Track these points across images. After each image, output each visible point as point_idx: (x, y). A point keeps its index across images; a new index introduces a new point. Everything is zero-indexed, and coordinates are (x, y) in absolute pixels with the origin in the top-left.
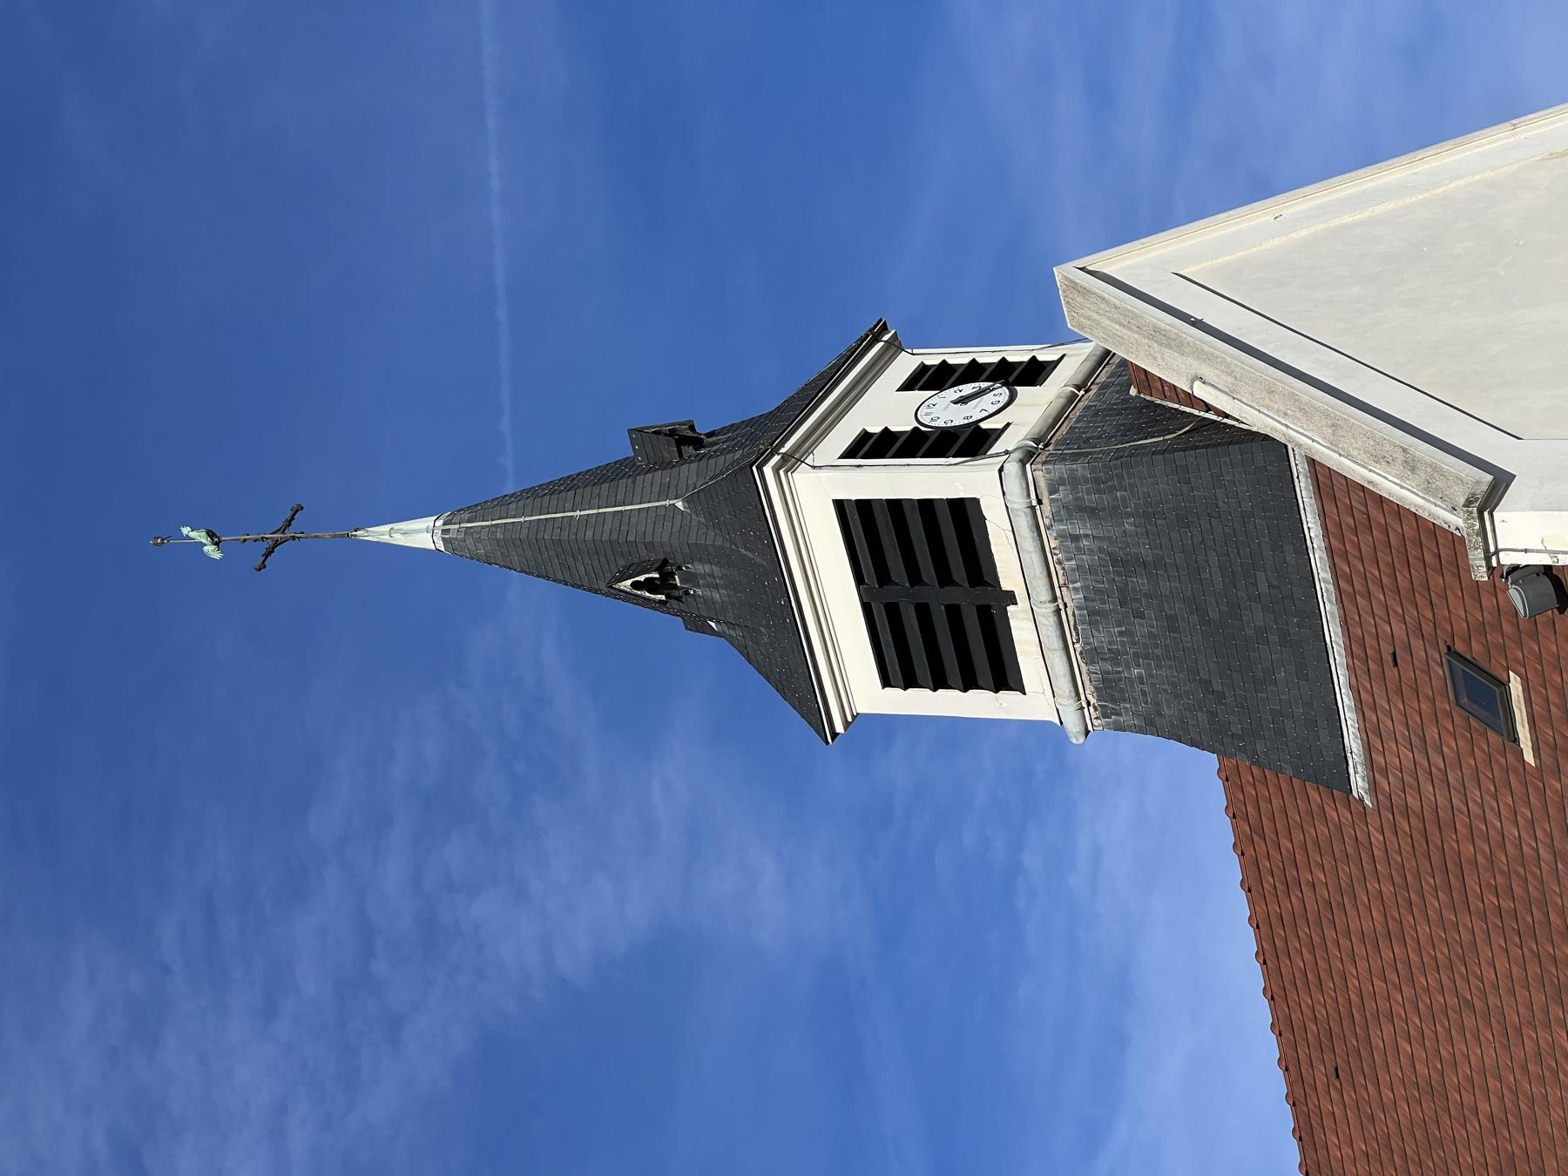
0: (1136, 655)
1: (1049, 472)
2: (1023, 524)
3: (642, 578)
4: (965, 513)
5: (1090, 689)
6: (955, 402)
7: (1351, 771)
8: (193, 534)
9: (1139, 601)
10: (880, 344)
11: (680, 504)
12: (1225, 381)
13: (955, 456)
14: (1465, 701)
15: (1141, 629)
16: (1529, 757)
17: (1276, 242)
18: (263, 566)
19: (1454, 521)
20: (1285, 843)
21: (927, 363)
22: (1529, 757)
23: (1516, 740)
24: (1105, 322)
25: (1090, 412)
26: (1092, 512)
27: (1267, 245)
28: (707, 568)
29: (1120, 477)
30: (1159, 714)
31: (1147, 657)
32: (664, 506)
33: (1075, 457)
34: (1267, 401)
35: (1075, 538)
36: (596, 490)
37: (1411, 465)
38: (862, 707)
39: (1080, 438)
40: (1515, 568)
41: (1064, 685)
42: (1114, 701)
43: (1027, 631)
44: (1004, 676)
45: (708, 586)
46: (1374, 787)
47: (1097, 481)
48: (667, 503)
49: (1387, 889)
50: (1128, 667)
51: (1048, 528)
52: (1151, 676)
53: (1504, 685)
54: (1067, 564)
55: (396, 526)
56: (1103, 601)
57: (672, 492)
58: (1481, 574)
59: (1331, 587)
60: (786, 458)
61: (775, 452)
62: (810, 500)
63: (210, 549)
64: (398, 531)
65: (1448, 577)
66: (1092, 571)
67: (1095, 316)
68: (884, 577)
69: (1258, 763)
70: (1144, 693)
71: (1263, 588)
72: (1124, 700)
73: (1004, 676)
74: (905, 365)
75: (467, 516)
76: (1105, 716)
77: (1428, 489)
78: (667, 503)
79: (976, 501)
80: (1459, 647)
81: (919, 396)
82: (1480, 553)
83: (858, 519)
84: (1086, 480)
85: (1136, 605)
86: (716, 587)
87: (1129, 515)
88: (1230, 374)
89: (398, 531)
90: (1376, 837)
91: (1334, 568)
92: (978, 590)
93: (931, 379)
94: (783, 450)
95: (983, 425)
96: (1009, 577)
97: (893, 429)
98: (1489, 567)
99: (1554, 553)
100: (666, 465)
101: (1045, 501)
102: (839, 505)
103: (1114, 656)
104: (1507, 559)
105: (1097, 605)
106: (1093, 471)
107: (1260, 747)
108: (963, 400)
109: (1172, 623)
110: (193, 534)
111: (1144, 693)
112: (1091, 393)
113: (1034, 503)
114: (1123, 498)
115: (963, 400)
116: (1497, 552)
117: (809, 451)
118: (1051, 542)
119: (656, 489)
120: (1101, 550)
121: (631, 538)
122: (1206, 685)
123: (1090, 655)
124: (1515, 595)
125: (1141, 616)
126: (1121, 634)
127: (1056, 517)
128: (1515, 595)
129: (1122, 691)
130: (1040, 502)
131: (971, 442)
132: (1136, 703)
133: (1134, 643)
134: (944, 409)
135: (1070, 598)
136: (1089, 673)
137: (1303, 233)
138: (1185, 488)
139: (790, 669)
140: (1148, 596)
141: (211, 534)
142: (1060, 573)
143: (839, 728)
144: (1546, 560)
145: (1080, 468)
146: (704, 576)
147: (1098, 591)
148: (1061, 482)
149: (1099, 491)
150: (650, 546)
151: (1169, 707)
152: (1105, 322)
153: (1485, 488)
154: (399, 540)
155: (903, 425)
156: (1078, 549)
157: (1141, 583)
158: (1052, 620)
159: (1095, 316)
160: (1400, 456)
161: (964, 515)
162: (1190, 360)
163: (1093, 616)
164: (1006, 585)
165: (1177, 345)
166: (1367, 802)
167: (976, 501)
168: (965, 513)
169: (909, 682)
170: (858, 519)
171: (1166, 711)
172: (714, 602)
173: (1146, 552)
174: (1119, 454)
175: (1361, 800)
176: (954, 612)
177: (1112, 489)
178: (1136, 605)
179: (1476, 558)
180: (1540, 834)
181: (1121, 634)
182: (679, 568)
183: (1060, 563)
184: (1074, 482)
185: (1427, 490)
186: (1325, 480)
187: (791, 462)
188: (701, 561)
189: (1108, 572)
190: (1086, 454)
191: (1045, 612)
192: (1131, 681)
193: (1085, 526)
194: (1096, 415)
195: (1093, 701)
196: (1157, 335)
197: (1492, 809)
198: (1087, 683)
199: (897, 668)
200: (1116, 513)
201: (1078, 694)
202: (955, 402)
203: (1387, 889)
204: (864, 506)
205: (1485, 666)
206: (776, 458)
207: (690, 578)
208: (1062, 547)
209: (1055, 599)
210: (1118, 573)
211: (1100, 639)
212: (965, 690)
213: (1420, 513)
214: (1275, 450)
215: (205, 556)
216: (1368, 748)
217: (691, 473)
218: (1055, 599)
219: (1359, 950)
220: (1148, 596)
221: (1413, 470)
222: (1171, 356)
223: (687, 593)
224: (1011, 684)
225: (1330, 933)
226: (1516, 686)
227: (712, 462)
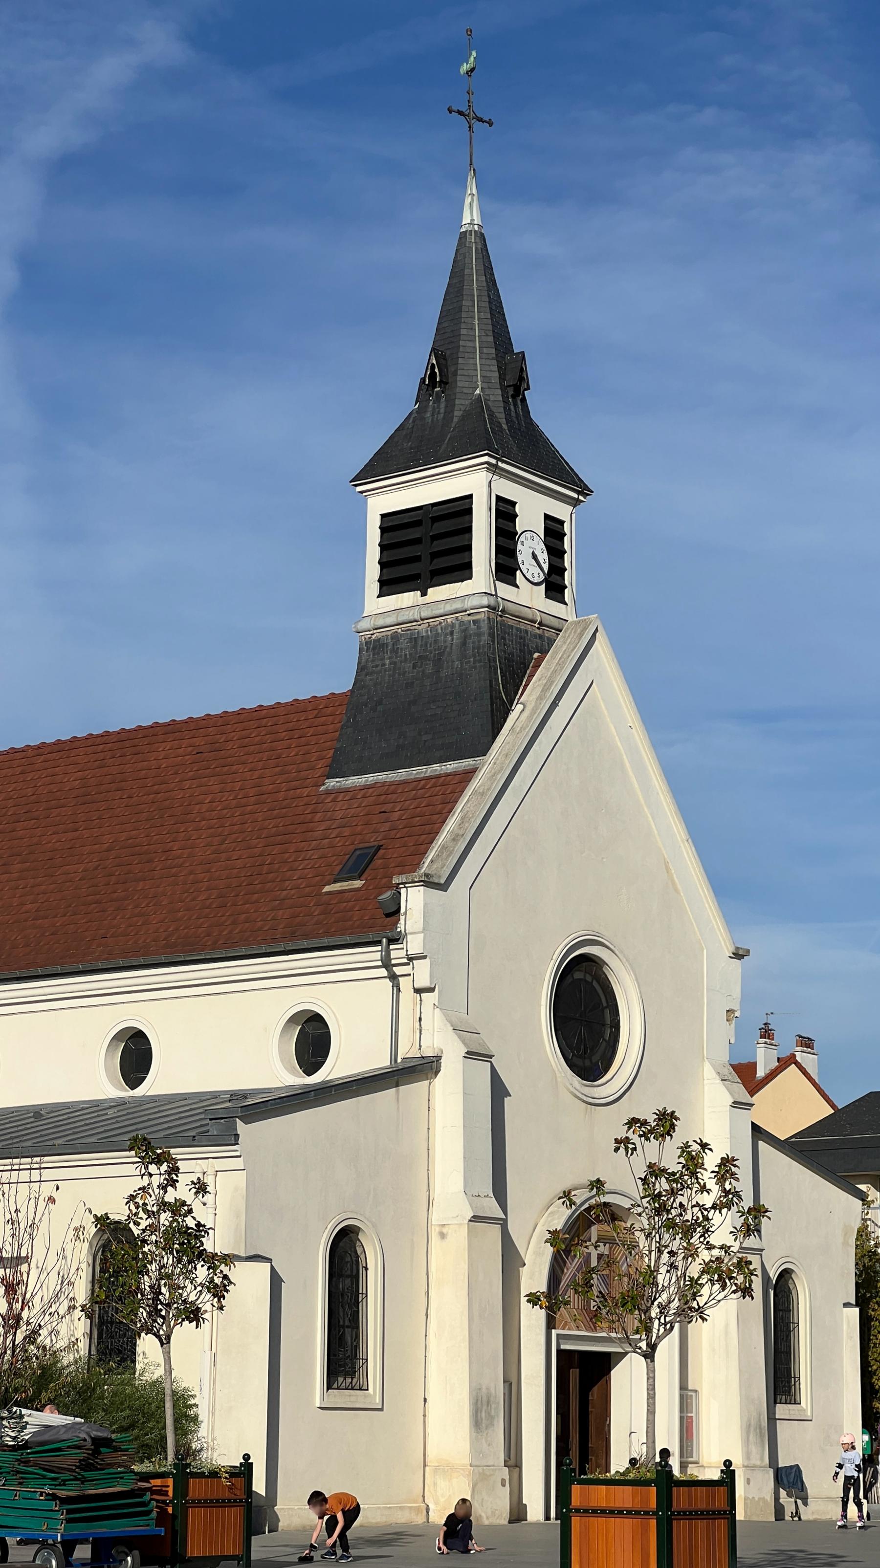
0: (395, 663)
1: (484, 620)
2: (458, 605)
3: (437, 370)
4: (464, 571)
5: (380, 635)
6: (533, 553)
7: (337, 780)
8: (472, 59)
9: (421, 667)
10: (576, 496)
11: (478, 392)
12: (519, 724)
13: (496, 563)
14: (358, 853)
15: (408, 666)
16: (327, 889)
17: (614, 730)
18: (450, 111)
19: (424, 868)
20: (311, 731)
21: (565, 524)
22: (327, 889)
23: (335, 882)
24: (564, 648)
25: (523, 634)
26: (464, 643)
27: (612, 727)
28: (442, 411)
29: (480, 661)
30: (366, 675)
31: (394, 669)
32: (478, 379)
33: (492, 635)
34: (504, 752)
35: (452, 633)
36: (491, 333)
37: (455, 838)
38: (371, 501)
39: (505, 633)
40: (400, 893)
41: (380, 622)
42: (374, 648)
43: (409, 598)
44: (388, 586)
45: (434, 408)
46: (328, 793)
47: (479, 648)
48: (479, 383)
49: (281, 795)
50: (390, 658)
51: (457, 618)
52: (385, 671)
53: (359, 877)
54: (439, 627)
55: (475, 198)
56: (421, 646)
57: (485, 385)
58: (395, 880)
59: (423, 775)
60: (496, 466)
61: (498, 459)
62: (469, 480)
63: (465, 67)
64: (472, 199)
65: (412, 848)
66: (436, 641)
67: (569, 640)
68: (435, 519)
69: (342, 728)
70: (377, 666)
71: (425, 738)
72: (374, 655)
73: (388, 586)
74: (561, 511)
75: (479, 247)
76: (366, 643)
77: (444, 847)
78: (479, 383)
79: (470, 578)
80: (381, 852)
81: (540, 528)
82: (404, 880)
83: (461, 508)
84: (479, 641)
85: (419, 664)
86: (433, 415)
87: (462, 664)
88: (521, 731)
89: (472, 199)
90: (306, 792)
91: (429, 778)
92: (428, 574)
93: (554, 531)
94: (500, 464)
95: (518, 573)
96: (437, 593)
97: (517, 520)
98: (399, 884)
99: (405, 914)
100: (502, 378)
101: (470, 618)
102: (470, 497)
103: (395, 651)
104: (403, 891)
105: (420, 643)
106: (484, 646)
107: (350, 730)
108: (534, 556)
109: (410, 685)
110: (472, 59)
111: (377, 666)
112: (537, 631)
113: (468, 612)
114: (469, 662)
115: (534, 556)
116: (407, 888)
117: (501, 476)
118: (450, 619)
119: (489, 374)
120: (446, 647)
121: (460, 361)
122: (380, 702)
123: (395, 637)
124: (387, 895)
125: (414, 667)
126: (406, 655)
127: (462, 623)
128: (387, 895)
129: (378, 654)
130: (469, 615)
131: (506, 568)
132: (373, 661)
133: (401, 662)
134: (531, 549)
135: (423, 627)
136: (387, 636)
137: (619, 744)
138: (473, 698)
139: (387, 463)
140: (423, 672)
141: (472, 70)
142: (435, 623)
143: (359, 489)
144: (403, 910)
145: (485, 638)
146: (439, 407)
147: (426, 643)
148: (479, 628)
149: (474, 648)
150: (455, 374)
151: (371, 680)
152: (564, 648)
153: (436, 881)
154: (468, 200)
155: (520, 525)
156: (446, 635)
157: (429, 668)
158: (411, 618)
159: (569, 640)
160: (461, 833)
161: (462, 570)
162: (533, 704)
163: (415, 639)
164: (430, 590)
165: (545, 689)
166: (322, 788)
167: (470, 578)
168: (464, 571)
169: (383, 530)
170: (461, 508)
171: (368, 678)
172: (426, 412)
173: (444, 673)
174: (491, 660)
175: (324, 784)
176: (417, 559)
177: (474, 655)
178: (419, 664)
179: (403, 878)
180: (293, 892)
181: (406, 655)
182: (443, 392)
183: (440, 623)
184: (479, 635)
185: (443, 846)
186: (468, 775)
187: (493, 469)
188: (446, 407)
189: (435, 650)
190: (493, 642)
191: (414, 614)
192: (383, 659)
193: (457, 639)
194: (521, 638)
195: (373, 637)
196: (550, 682)
197: (307, 865)
198: (382, 634)
199: (392, 523)
200: (463, 656)
201: (376, 629)
202: (533, 553)
203: (281, 795)
204: (469, 511)
205: (370, 866)
206: (494, 461)
207: (438, 400)
208: (448, 625)
209: (422, 620)
210: (434, 657)
211: (404, 644)
212: (379, 563)
213: (433, 845)
214: (484, 751)
215: (462, 64)
216: (346, 791)
217: (496, 395)
218: (422, 620)
219: (257, 774)
220: (423, 672)
221: (454, 840)
222: (534, 697)
223: (431, 396)
224: (384, 588)
225: (265, 756)
226: (358, 884)
227: (502, 410)
